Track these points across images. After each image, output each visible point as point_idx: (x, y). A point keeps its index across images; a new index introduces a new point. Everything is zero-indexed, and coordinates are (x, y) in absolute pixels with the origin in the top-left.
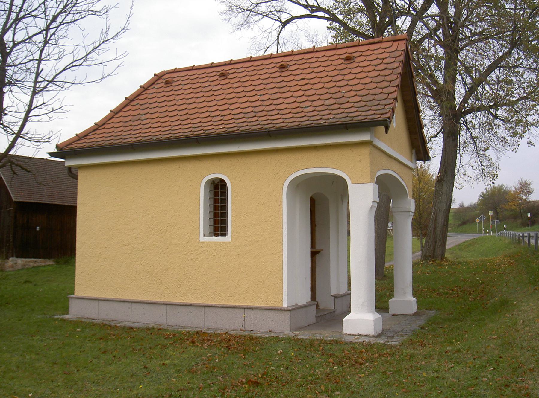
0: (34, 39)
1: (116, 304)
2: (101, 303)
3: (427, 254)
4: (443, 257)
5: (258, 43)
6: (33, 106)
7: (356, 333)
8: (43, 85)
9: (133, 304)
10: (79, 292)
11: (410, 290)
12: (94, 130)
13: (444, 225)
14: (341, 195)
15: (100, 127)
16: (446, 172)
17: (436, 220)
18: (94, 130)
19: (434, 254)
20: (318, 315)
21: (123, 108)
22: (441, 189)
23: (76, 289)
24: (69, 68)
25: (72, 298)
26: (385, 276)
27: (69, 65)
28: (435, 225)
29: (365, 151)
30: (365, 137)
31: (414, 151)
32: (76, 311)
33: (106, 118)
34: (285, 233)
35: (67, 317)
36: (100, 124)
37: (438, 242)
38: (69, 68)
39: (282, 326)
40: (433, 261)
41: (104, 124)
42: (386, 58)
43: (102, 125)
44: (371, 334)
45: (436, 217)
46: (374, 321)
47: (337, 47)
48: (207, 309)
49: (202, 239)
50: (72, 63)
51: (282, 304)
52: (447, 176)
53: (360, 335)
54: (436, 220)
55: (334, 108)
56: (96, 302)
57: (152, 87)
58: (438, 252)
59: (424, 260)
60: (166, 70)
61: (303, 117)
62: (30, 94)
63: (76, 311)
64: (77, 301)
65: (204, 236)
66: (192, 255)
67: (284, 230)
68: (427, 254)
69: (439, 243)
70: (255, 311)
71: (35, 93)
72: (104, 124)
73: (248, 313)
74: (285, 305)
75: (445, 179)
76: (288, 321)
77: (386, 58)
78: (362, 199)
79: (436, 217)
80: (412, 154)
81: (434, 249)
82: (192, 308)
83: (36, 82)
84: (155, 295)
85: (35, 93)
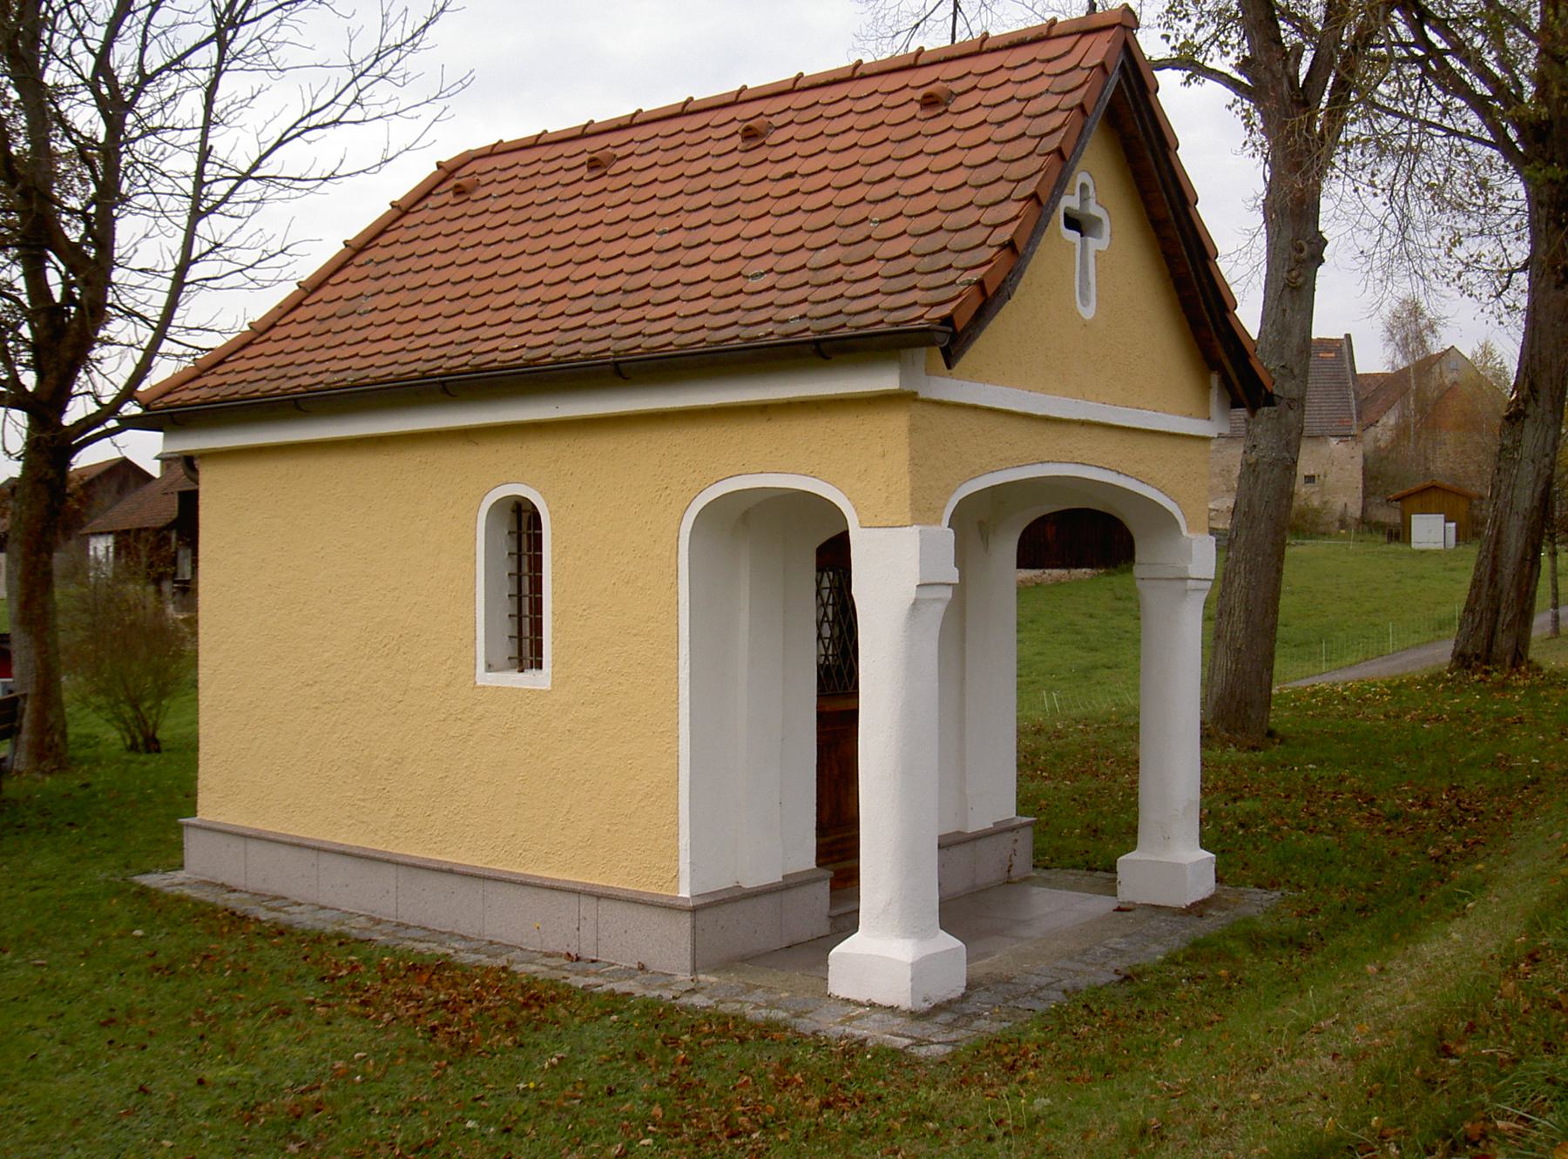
0: (192, 60)
1: (283, 851)
2: (254, 846)
3: (1469, 650)
4: (1519, 656)
5: (894, 11)
6: (194, 255)
7: (863, 998)
8: (220, 189)
9: (325, 857)
10: (211, 807)
11: (1188, 826)
12: (244, 347)
13: (1523, 559)
14: (981, 523)
15: (261, 334)
16: (1533, 389)
17: (1498, 542)
18: (244, 347)
19: (1489, 650)
20: (836, 912)
21: (331, 276)
22: (1517, 444)
23: (203, 799)
24: (298, 135)
25: (188, 825)
26: (1271, 734)
27: (294, 127)
28: (1495, 558)
29: (897, 423)
30: (886, 380)
31: (1215, 379)
32: (203, 866)
33: (280, 306)
34: (684, 674)
35: (180, 876)
36: (261, 328)
37: (1503, 611)
38: (298, 135)
39: (659, 960)
40: (1487, 672)
41: (274, 326)
42: (1035, 97)
43: (267, 330)
44: (904, 1008)
45: (1499, 532)
46: (916, 966)
47: (920, 62)
48: (489, 886)
49: (485, 678)
50: (303, 119)
51: (677, 888)
52: (1536, 400)
53: (872, 1005)
54: (1498, 542)
55: (827, 280)
56: (240, 842)
57: (420, 206)
58: (1505, 642)
59: (1457, 668)
60: (474, 148)
61: (730, 311)
62: (183, 220)
63: (203, 866)
64: (199, 833)
65: (489, 667)
66: (459, 723)
67: (681, 662)
68: (1469, 650)
69: (1506, 616)
70: (604, 903)
71: (196, 215)
72: (274, 326)
73: (588, 905)
74: (685, 892)
75: (1530, 410)
76: (685, 943)
77: (1035, 97)
78: (894, 572)
79: (1499, 532)
80: (1206, 387)
81: (1492, 635)
82: (456, 879)
83: (199, 183)
84: (375, 832)
85: (196, 215)
